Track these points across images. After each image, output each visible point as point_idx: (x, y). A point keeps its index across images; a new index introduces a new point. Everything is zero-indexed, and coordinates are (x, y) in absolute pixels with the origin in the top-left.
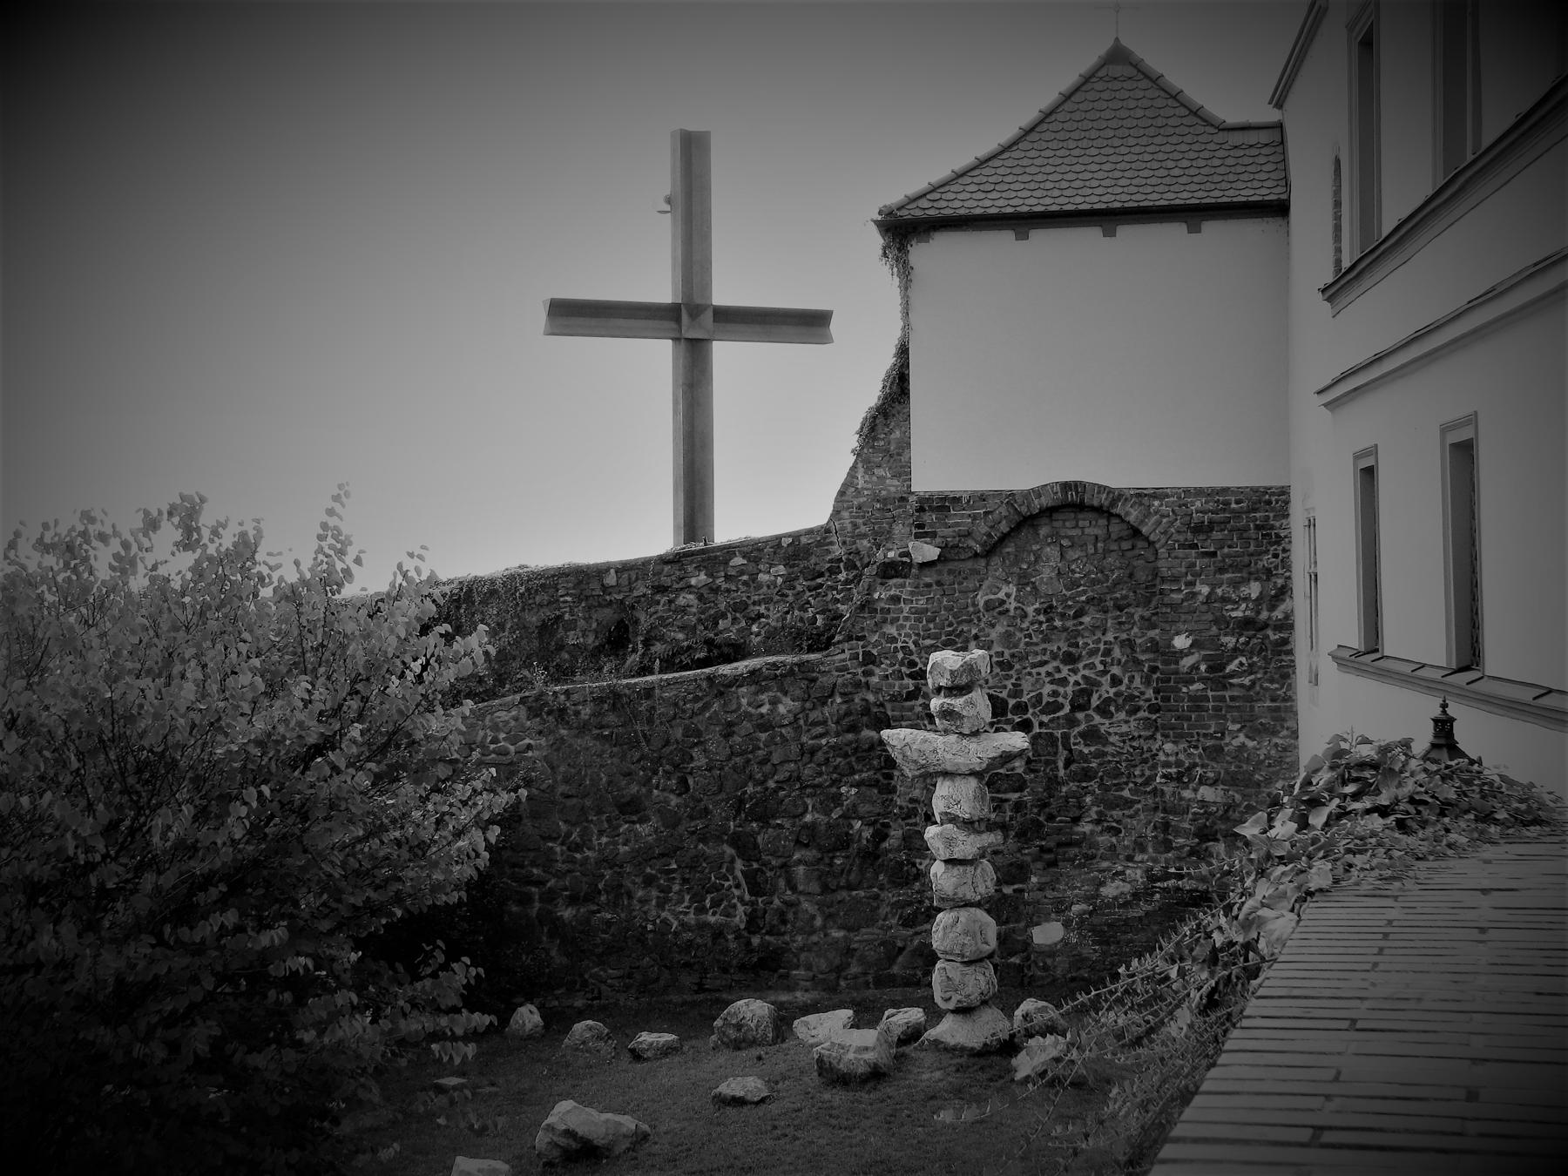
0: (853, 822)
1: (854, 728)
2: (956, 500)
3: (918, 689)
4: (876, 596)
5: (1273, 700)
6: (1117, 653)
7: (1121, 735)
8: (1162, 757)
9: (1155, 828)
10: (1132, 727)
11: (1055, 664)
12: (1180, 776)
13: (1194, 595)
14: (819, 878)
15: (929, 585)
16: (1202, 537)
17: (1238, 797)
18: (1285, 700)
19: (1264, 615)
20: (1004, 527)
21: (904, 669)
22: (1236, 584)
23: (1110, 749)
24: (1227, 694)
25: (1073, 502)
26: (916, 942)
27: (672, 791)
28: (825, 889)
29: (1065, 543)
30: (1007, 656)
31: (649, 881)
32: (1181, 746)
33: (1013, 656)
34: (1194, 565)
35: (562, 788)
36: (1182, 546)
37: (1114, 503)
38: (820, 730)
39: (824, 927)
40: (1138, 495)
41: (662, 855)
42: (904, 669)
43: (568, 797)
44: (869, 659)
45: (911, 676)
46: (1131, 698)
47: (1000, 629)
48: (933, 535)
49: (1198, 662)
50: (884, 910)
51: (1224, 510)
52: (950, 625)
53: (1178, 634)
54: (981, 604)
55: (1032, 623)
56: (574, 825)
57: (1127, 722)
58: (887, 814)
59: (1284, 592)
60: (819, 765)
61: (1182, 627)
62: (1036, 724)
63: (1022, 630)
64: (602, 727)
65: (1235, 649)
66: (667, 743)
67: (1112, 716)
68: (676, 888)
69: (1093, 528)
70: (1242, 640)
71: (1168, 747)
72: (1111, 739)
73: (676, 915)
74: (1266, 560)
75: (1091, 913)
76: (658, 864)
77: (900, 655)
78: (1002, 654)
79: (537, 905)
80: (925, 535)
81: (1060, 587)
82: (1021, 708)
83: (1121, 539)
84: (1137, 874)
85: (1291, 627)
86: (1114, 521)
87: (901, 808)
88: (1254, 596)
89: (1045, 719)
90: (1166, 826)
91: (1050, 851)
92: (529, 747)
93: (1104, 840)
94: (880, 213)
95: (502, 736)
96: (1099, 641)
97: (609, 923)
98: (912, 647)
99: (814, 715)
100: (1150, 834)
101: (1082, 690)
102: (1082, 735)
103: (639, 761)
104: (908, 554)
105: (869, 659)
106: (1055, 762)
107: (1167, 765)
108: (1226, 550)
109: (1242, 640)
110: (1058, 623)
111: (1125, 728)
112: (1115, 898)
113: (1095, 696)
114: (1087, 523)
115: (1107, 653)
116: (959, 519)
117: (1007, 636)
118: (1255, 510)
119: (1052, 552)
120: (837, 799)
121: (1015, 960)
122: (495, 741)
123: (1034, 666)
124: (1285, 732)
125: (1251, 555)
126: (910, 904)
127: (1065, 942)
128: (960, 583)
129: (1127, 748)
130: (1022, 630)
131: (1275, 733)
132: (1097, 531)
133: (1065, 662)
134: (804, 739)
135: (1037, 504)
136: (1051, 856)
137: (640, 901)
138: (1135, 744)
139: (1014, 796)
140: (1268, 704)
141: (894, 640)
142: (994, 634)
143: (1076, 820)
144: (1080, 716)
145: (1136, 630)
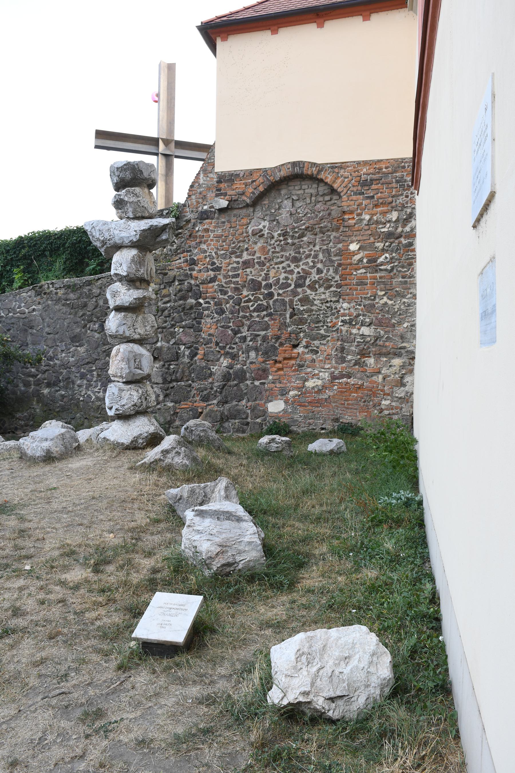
0: (181, 346)
1: (184, 298)
2: (238, 175)
3: (215, 276)
4: (197, 229)
5: (403, 277)
6: (321, 256)
7: (321, 300)
8: (342, 311)
9: (336, 350)
10: (327, 296)
11: (287, 262)
12: (351, 321)
13: (362, 220)
14: (162, 375)
15: (224, 222)
16: (366, 188)
17: (382, 332)
18: (410, 277)
19: (400, 229)
20: (261, 189)
21: (209, 266)
22: (384, 213)
23: (314, 308)
24: (378, 275)
25: (298, 175)
26: (208, 409)
27: (96, 331)
28: (165, 381)
29: (295, 198)
30: (262, 259)
31: (83, 376)
32: (352, 305)
33: (265, 258)
34: (362, 203)
35: (47, 330)
36: (355, 194)
37: (319, 172)
38: (167, 299)
39: (164, 401)
40: (332, 168)
41: (88, 363)
42: (209, 266)
43: (49, 334)
44: (193, 262)
45: (212, 270)
46: (328, 280)
47: (259, 245)
48: (225, 194)
49: (362, 258)
50: (194, 392)
51: (379, 173)
52: (234, 243)
53: (352, 242)
54: (250, 232)
55: (276, 242)
56: (51, 347)
57: (324, 293)
58: (197, 342)
59: (411, 216)
60: (166, 317)
61: (354, 238)
62: (276, 295)
63: (270, 245)
64: (67, 300)
65: (383, 250)
66: (96, 307)
67: (317, 290)
68: (95, 379)
69: (310, 189)
70: (387, 244)
71: (345, 305)
72: (315, 302)
73: (94, 393)
74: (401, 200)
75: (299, 396)
76: (87, 367)
77: (208, 259)
78: (260, 257)
79: (33, 387)
80: (221, 194)
81: (290, 221)
82: (269, 286)
83: (324, 195)
84: (326, 376)
85: (414, 236)
86: (321, 184)
87: (203, 338)
88: (394, 219)
89: (281, 292)
90: (342, 349)
91: (280, 362)
92: (34, 310)
93: (309, 356)
94: (202, 23)
95: (23, 304)
96: (311, 250)
97: (63, 396)
98: (214, 254)
99: (164, 292)
100: (333, 353)
101: (301, 277)
102: (300, 300)
103: (82, 316)
104: (212, 207)
105: (193, 262)
106: (285, 315)
107: (344, 315)
108: (379, 195)
109: (387, 244)
110: (290, 241)
111: (323, 296)
112: (313, 388)
113: (308, 280)
114: (306, 187)
115: (316, 256)
116: (239, 186)
117: (263, 248)
118: (395, 171)
119: (287, 203)
120: (173, 335)
121: (259, 420)
122: (19, 307)
123: (276, 264)
124: (409, 296)
125: (393, 197)
126: (206, 390)
127: (285, 411)
128: (240, 221)
129: (324, 307)
130: (270, 245)
131: (404, 297)
132: (313, 191)
133: (292, 262)
134: (159, 304)
135: (278, 176)
136: (280, 365)
137: (78, 386)
138: (328, 305)
139: (263, 333)
140: (400, 279)
141: (205, 252)
142: (257, 247)
143: (295, 346)
144: (299, 290)
145: (331, 244)
